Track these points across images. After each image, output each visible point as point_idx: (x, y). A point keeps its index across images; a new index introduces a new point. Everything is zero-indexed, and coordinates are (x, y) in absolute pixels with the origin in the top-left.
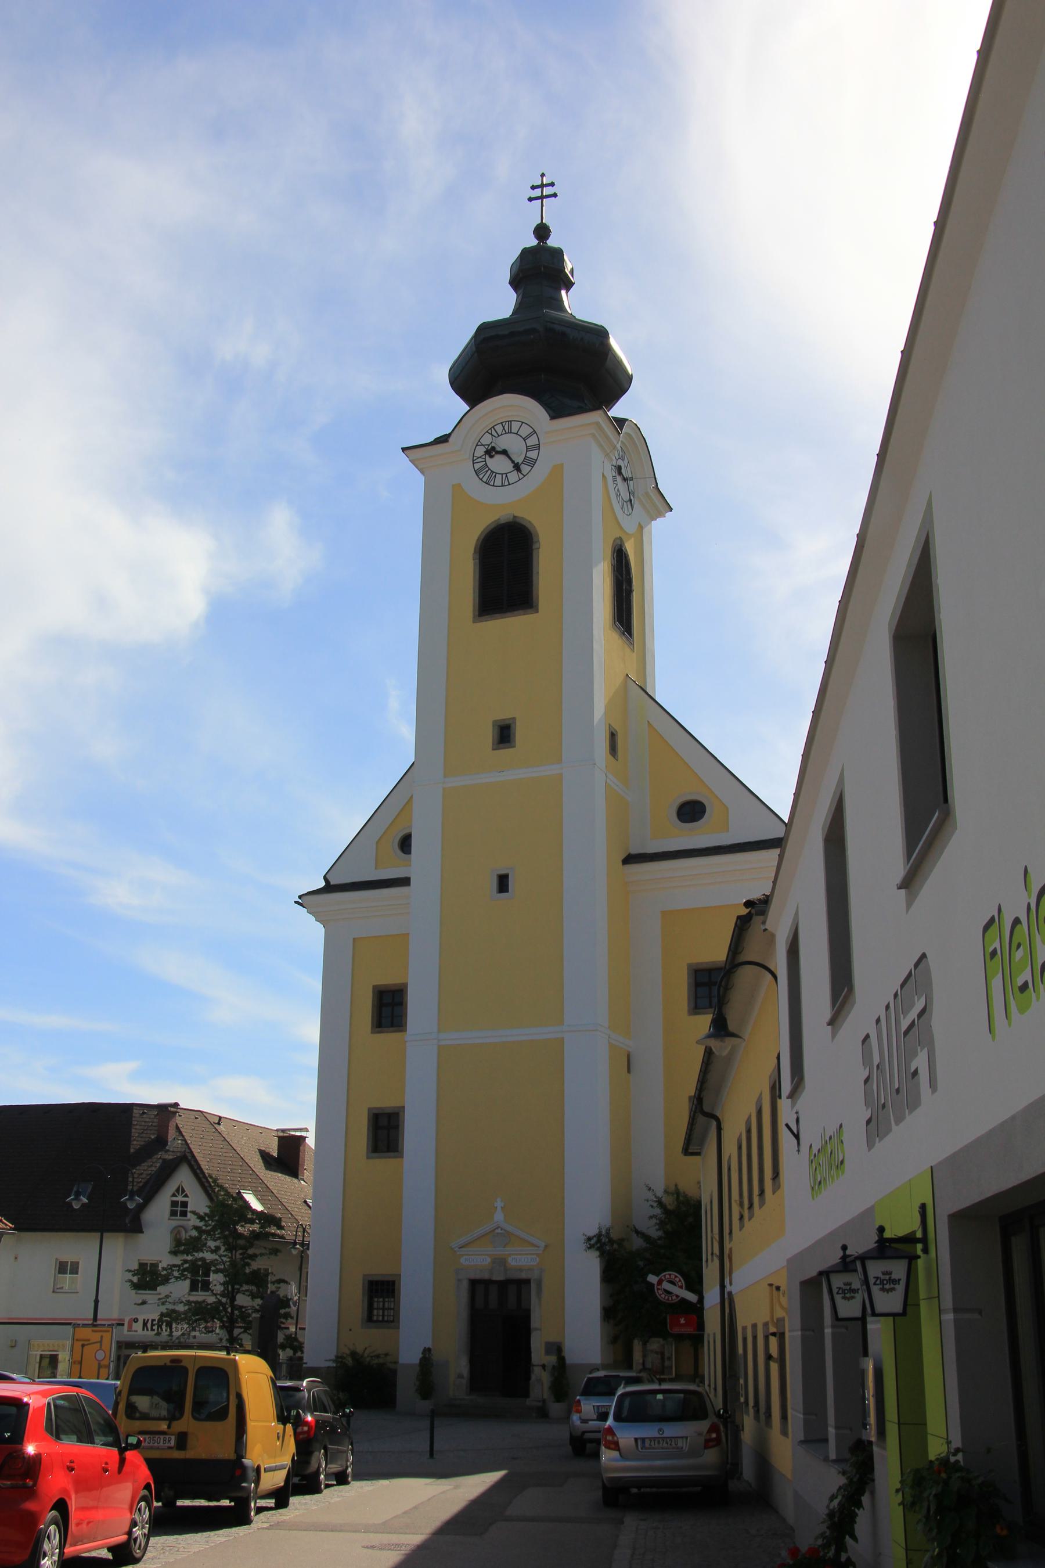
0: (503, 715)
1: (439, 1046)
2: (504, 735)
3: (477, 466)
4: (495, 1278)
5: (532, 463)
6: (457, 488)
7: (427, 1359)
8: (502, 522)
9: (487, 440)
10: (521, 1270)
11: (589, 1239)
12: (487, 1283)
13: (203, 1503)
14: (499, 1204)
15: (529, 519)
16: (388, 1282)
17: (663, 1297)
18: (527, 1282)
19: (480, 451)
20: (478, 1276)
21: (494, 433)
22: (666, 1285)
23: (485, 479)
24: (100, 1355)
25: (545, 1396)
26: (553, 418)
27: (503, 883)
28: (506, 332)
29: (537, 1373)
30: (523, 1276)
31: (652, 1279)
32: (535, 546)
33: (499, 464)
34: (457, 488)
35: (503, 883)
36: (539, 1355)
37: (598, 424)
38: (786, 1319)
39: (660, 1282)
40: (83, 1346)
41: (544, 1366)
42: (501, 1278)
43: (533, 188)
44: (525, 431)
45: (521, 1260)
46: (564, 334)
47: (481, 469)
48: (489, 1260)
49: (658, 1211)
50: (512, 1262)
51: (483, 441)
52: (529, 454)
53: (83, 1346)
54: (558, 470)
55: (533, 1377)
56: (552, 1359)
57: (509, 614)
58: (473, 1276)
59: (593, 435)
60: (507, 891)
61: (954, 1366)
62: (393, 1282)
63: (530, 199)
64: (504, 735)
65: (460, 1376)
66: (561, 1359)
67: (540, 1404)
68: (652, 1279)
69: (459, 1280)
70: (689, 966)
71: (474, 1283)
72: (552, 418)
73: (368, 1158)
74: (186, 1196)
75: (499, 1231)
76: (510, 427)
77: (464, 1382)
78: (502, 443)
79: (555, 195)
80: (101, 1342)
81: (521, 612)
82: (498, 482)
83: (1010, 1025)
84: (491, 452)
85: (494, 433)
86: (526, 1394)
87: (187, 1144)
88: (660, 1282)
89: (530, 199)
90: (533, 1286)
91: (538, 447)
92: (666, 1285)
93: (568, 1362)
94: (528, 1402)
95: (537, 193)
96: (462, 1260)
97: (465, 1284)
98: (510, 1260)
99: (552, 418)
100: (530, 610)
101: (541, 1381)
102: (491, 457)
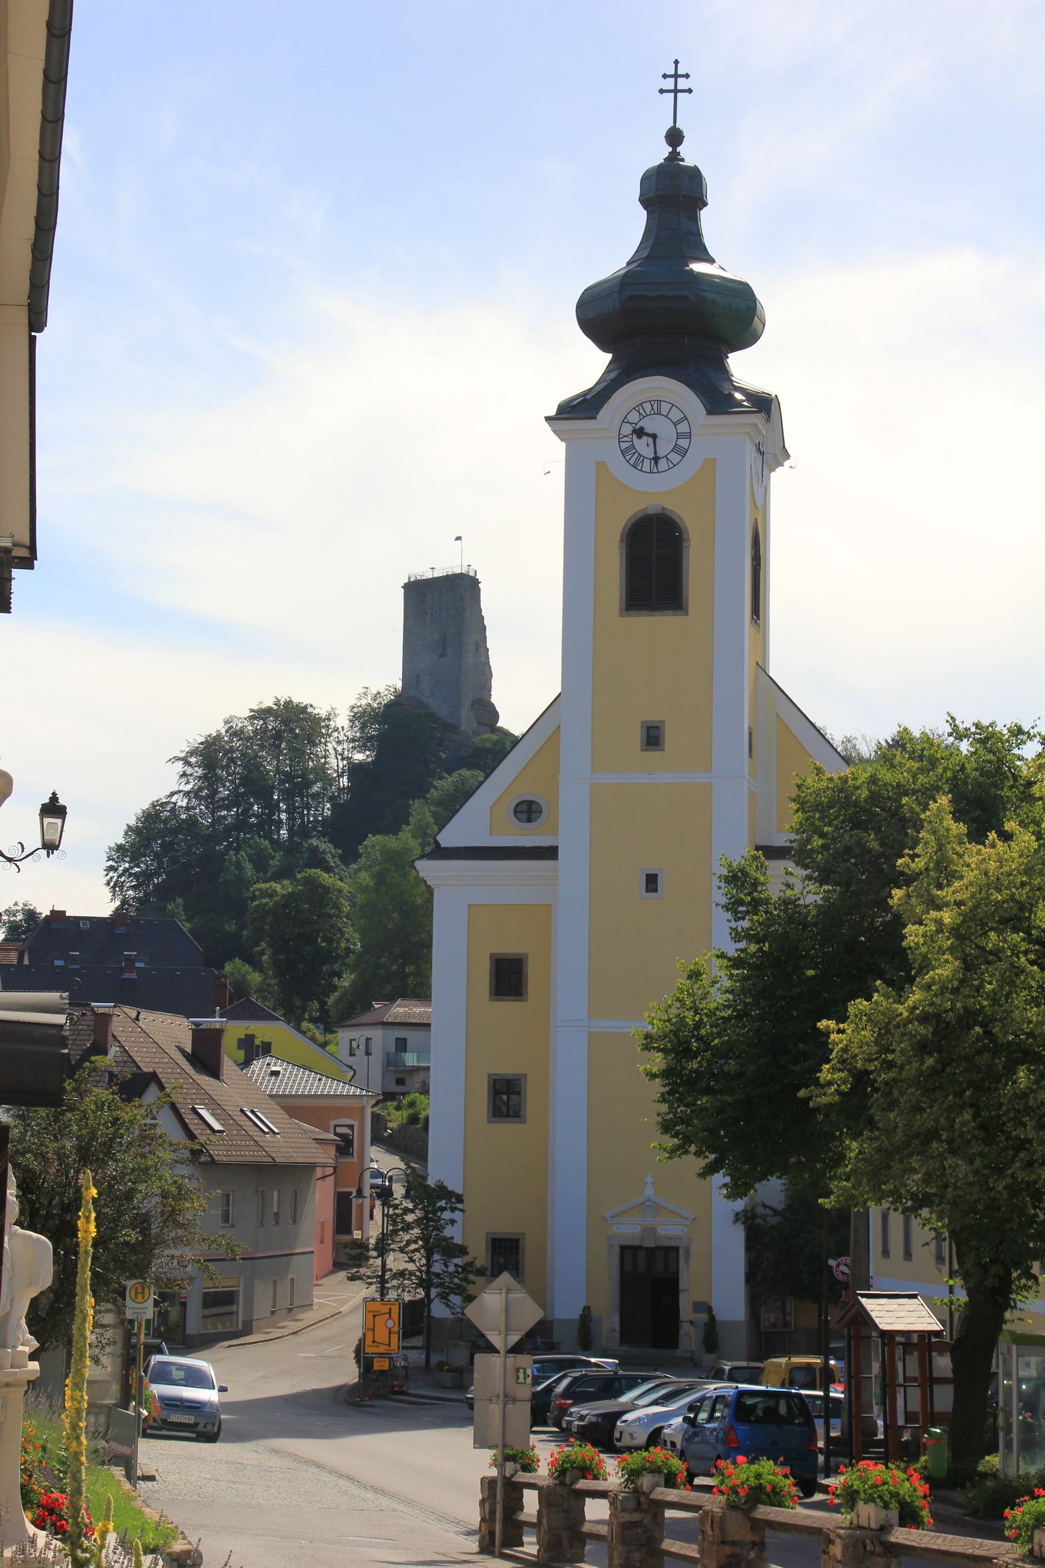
0: (653, 716)
1: (590, 1033)
2: (653, 737)
3: (624, 446)
4: (645, 1245)
5: (683, 452)
6: (601, 465)
7: (586, 1316)
8: (651, 512)
9: (634, 417)
10: (670, 1238)
11: (737, 1214)
12: (635, 1249)
13: (803, 1392)
14: (649, 1179)
15: (679, 513)
16: (512, 1240)
18: (676, 1249)
19: (627, 429)
20: (629, 1243)
21: (642, 411)
23: (632, 462)
24: (390, 1324)
25: (693, 1348)
26: (710, 412)
27: (652, 882)
28: (654, 294)
29: (685, 1329)
30: (673, 1244)
31: (832, 1262)
32: (685, 544)
33: (643, 445)
34: (601, 465)
35: (652, 882)
36: (686, 1311)
37: (755, 425)
39: (838, 1265)
40: (374, 1316)
41: (692, 1323)
42: (652, 1245)
43: (665, 76)
44: (675, 415)
45: (669, 1231)
47: (628, 449)
48: (639, 1229)
50: (661, 1231)
51: (630, 418)
52: (680, 442)
53: (374, 1316)
54: (710, 464)
55: (682, 1332)
56: (703, 1317)
57: (657, 613)
58: (624, 1243)
59: (748, 433)
60: (648, 876)
63: (662, 91)
64: (653, 737)
65: (613, 1330)
66: (712, 1318)
67: (689, 1355)
68: (832, 1262)
69: (611, 1246)
71: (623, 1248)
72: (709, 413)
73: (489, 1122)
74: (155, 1118)
75: (650, 1203)
76: (659, 408)
77: (617, 1335)
78: (649, 426)
79: (690, 91)
80: (390, 1313)
81: (670, 612)
84: (640, 433)
85: (642, 411)
86: (675, 1345)
87: (127, 1052)
88: (838, 1265)
90: (681, 1253)
91: (689, 435)
93: (717, 1318)
94: (678, 1352)
95: (669, 84)
96: (614, 1228)
97: (617, 1249)
98: (659, 1229)
99: (710, 412)
100: (679, 612)
101: (690, 1337)
102: (639, 437)
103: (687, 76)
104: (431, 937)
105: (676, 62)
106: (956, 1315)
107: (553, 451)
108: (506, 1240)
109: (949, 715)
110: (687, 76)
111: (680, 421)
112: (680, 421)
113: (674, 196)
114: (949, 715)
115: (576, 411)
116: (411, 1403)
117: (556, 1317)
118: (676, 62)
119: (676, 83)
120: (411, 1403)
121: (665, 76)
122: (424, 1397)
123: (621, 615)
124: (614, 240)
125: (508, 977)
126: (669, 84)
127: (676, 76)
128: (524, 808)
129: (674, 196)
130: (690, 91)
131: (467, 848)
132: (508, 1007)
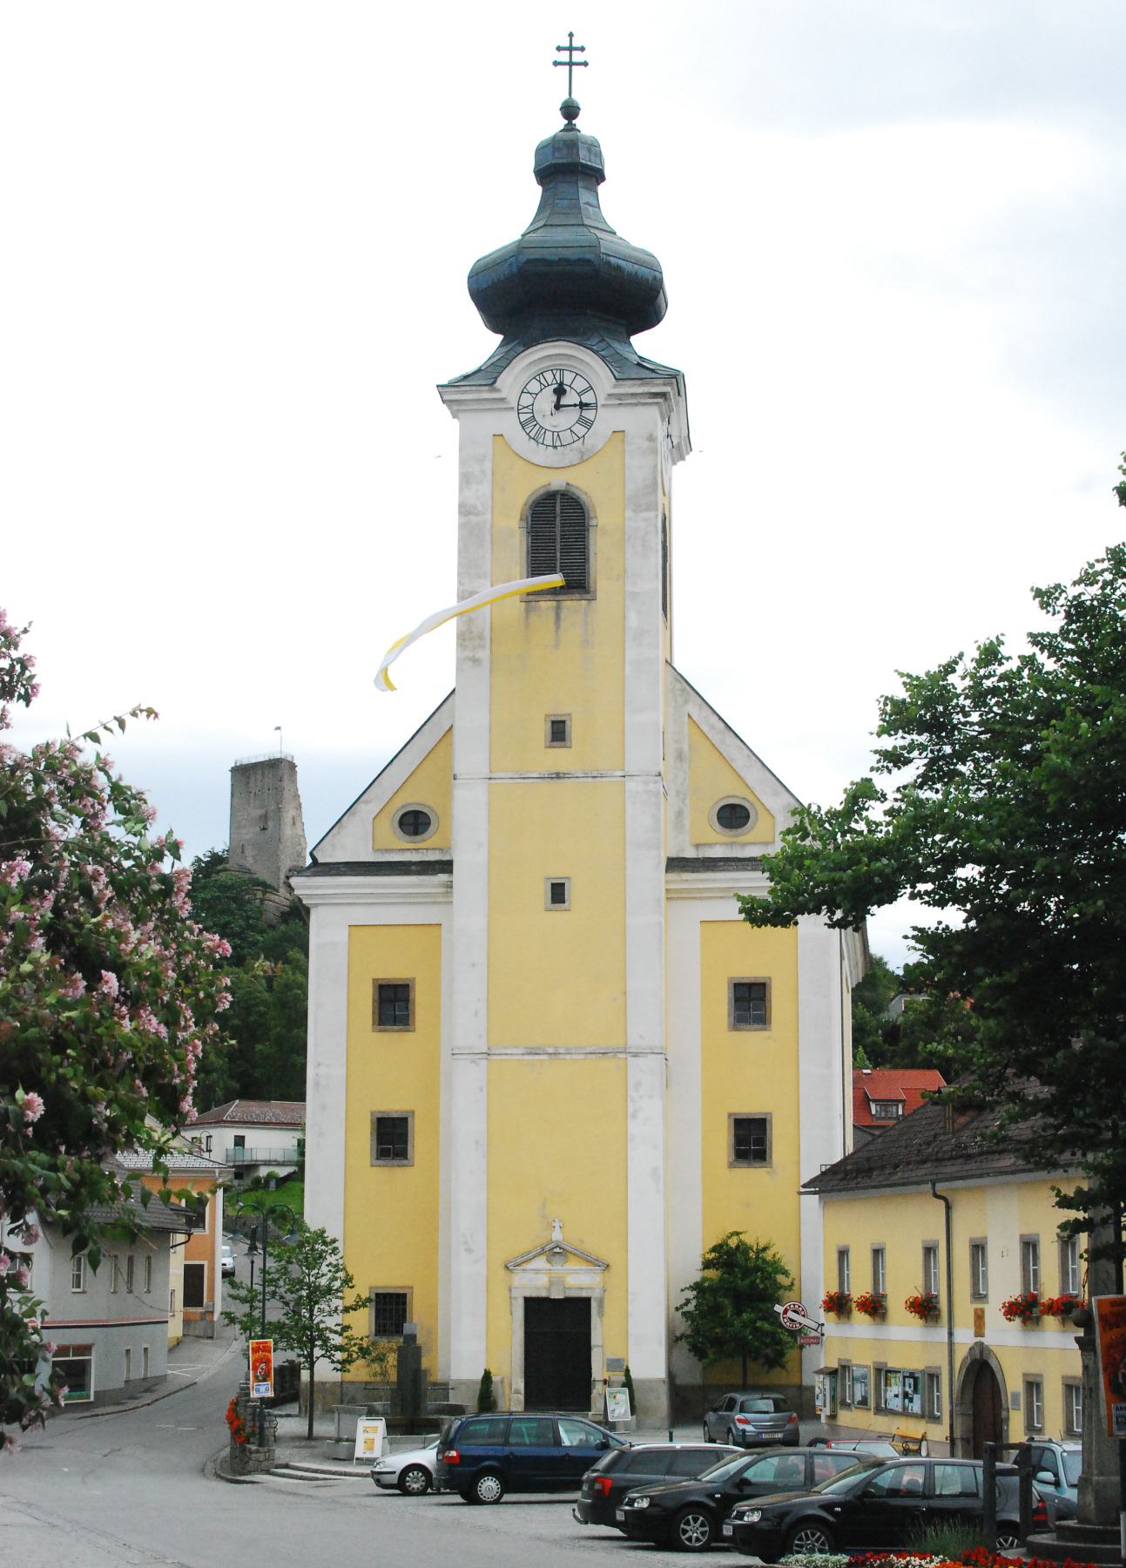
17: (788, 1325)
18: (587, 1301)
22: (791, 1314)
30: (584, 1294)
38: (200, 1310)
39: (786, 1312)
43: (559, 49)
46: (619, 268)
47: (527, 421)
49: (762, 1245)
61: (542, 1411)
62: (404, 1295)
63: (556, 64)
65: (517, 1392)
70: (730, 979)
79: (585, 64)
82: (548, 441)
83: (557, 646)
88: (786, 1312)
89: (556, 64)
90: (594, 1305)
92: (791, 1314)
95: (564, 57)
103: (582, 49)
104: (306, 994)
105: (571, 35)
106: (957, 1365)
107: (445, 429)
108: (391, 1295)
109: (902, 675)
110: (582, 49)
111: (585, 391)
112: (585, 391)
113: (568, 169)
114: (902, 675)
115: (466, 392)
116: (301, 1478)
117: (454, 1377)
118: (571, 35)
119: (570, 56)
120: (301, 1478)
121: (559, 49)
122: (307, 1470)
123: (372, 1113)
124: (505, 212)
125: (394, 1004)
126: (564, 57)
127: (571, 49)
128: (411, 819)
129: (568, 169)
130: (585, 64)
131: (346, 864)
132: (393, 1039)
